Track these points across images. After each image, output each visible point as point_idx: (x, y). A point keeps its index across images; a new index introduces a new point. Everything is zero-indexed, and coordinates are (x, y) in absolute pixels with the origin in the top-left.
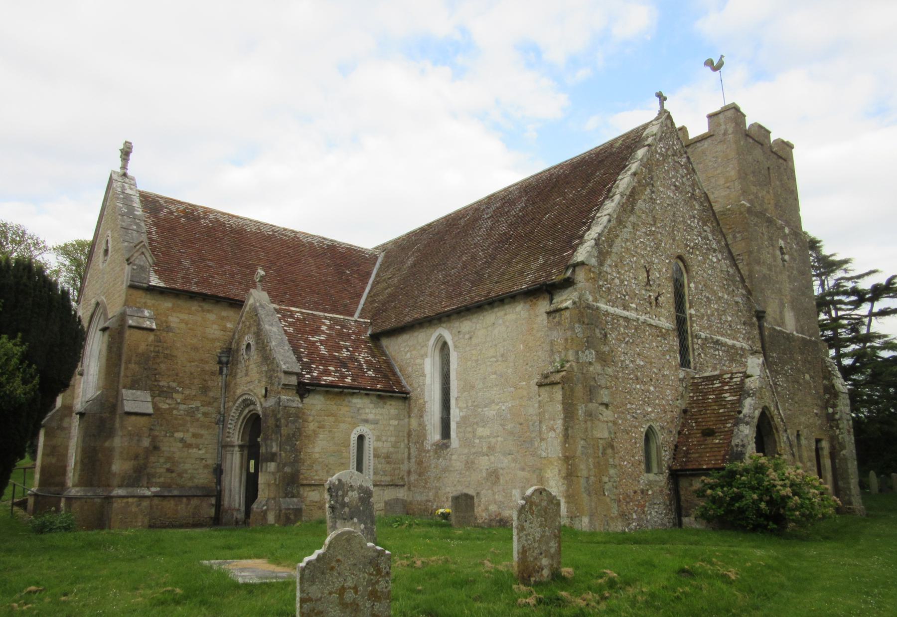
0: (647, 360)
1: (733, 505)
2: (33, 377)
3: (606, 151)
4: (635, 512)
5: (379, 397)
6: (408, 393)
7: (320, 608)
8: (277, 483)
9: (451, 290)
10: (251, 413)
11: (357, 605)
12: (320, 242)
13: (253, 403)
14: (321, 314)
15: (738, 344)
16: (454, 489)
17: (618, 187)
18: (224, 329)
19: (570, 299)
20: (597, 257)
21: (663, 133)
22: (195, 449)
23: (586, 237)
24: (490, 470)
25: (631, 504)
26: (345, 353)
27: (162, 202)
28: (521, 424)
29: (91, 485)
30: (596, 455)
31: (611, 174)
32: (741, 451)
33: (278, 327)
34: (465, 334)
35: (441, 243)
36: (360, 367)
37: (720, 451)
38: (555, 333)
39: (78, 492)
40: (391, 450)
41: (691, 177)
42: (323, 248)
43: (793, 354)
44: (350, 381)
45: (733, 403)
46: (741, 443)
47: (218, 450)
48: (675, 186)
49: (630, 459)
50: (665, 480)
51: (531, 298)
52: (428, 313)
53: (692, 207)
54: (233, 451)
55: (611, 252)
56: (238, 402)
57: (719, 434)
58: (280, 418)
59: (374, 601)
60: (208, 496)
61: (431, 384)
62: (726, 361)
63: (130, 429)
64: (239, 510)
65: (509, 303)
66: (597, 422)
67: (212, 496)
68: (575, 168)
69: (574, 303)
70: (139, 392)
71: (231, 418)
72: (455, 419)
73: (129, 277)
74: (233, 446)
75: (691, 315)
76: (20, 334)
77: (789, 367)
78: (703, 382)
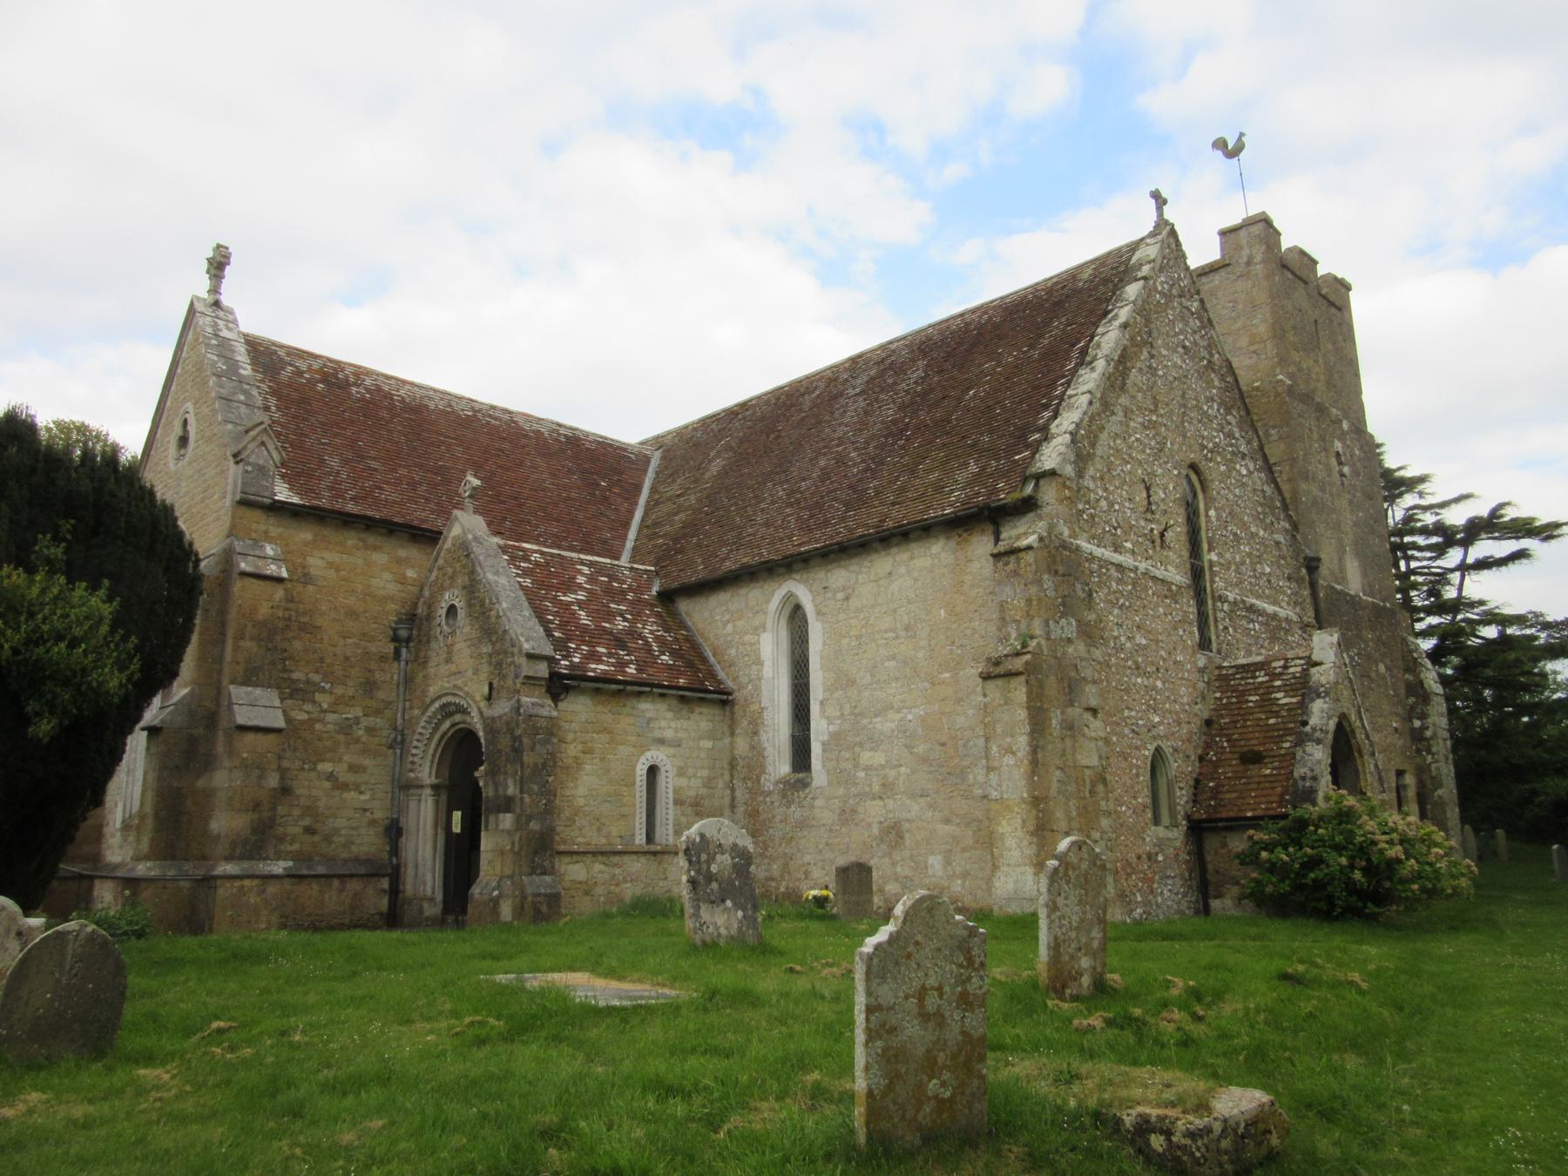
0: (1151, 637)
1: (1304, 876)
2: (131, 658)
3: (1065, 286)
4: (1139, 890)
5: (683, 699)
6: (729, 694)
7: (893, 1021)
8: (516, 849)
9: (805, 515)
10: (456, 728)
11: (942, 1016)
12: (554, 431)
13: (464, 711)
14: (574, 555)
15: (1282, 613)
16: (819, 858)
17: (1098, 345)
18: (402, 581)
19: (1034, 533)
20: (1074, 462)
21: (1164, 258)
22: (353, 793)
23: (1053, 428)
24: (885, 825)
25: (1134, 877)
26: (621, 624)
27: (281, 353)
28: (943, 745)
29: (174, 858)
30: (1082, 795)
31: (1082, 324)
32: (1312, 787)
33: (508, 576)
34: (836, 591)
35: (772, 436)
36: (645, 647)
37: (1274, 788)
38: (1008, 590)
39: (150, 869)
40: (703, 791)
41: (1206, 334)
42: (560, 442)
43: (1360, 631)
44: (634, 672)
45: (1290, 708)
46: (1309, 774)
47: (393, 792)
48: (1184, 347)
49: (1130, 803)
50: (1181, 838)
51: (960, 531)
52: (766, 554)
53: (1209, 384)
54: (420, 795)
55: (1094, 454)
56: (432, 709)
57: (1271, 760)
58: (520, 736)
59: (965, 1010)
60: (376, 875)
61: (773, 678)
62: (1264, 640)
63: (245, 755)
64: (432, 900)
65: (918, 539)
66: (1081, 740)
67: (383, 876)
68: (1011, 313)
69: (1041, 539)
70: (258, 691)
71: (416, 737)
72: (821, 738)
73: (239, 485)
74: (421, 787)
75: (1211, 564)
76: (106, 582)
77: (1356, 651)
78: (1237, 673)
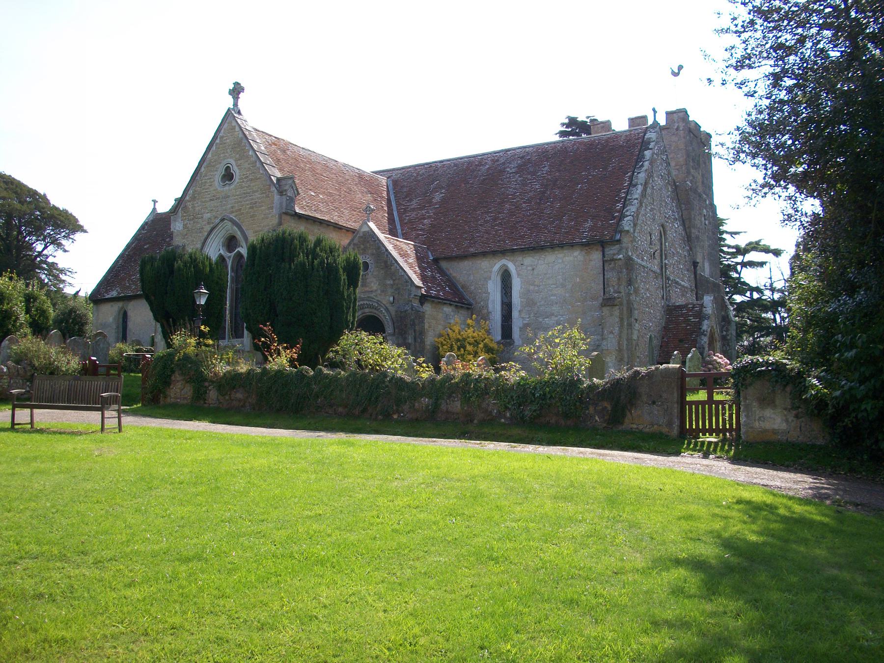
6: (471, 305)
